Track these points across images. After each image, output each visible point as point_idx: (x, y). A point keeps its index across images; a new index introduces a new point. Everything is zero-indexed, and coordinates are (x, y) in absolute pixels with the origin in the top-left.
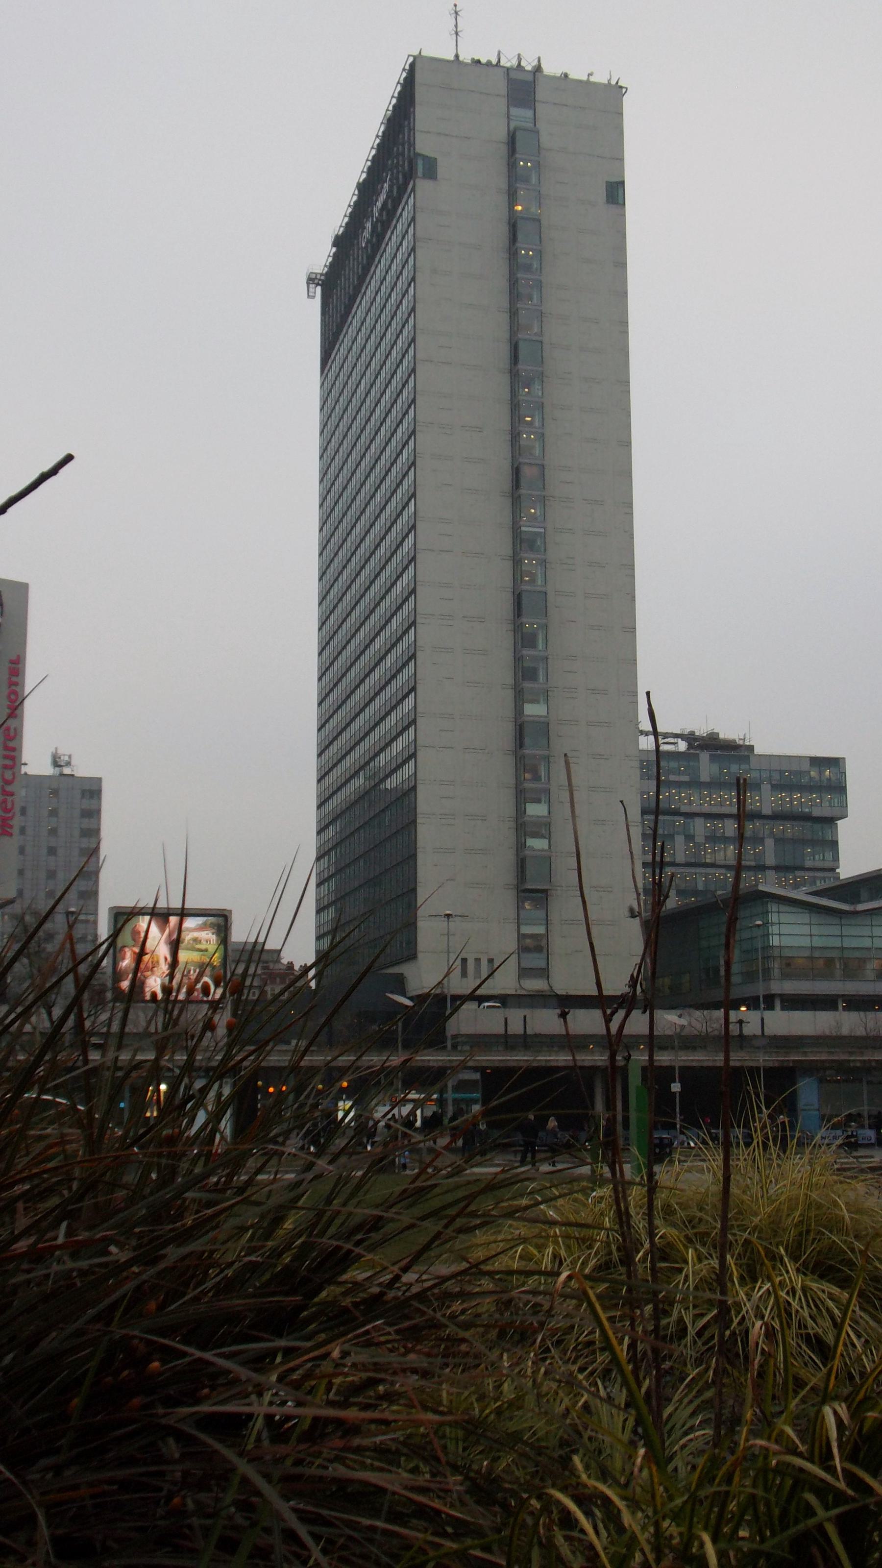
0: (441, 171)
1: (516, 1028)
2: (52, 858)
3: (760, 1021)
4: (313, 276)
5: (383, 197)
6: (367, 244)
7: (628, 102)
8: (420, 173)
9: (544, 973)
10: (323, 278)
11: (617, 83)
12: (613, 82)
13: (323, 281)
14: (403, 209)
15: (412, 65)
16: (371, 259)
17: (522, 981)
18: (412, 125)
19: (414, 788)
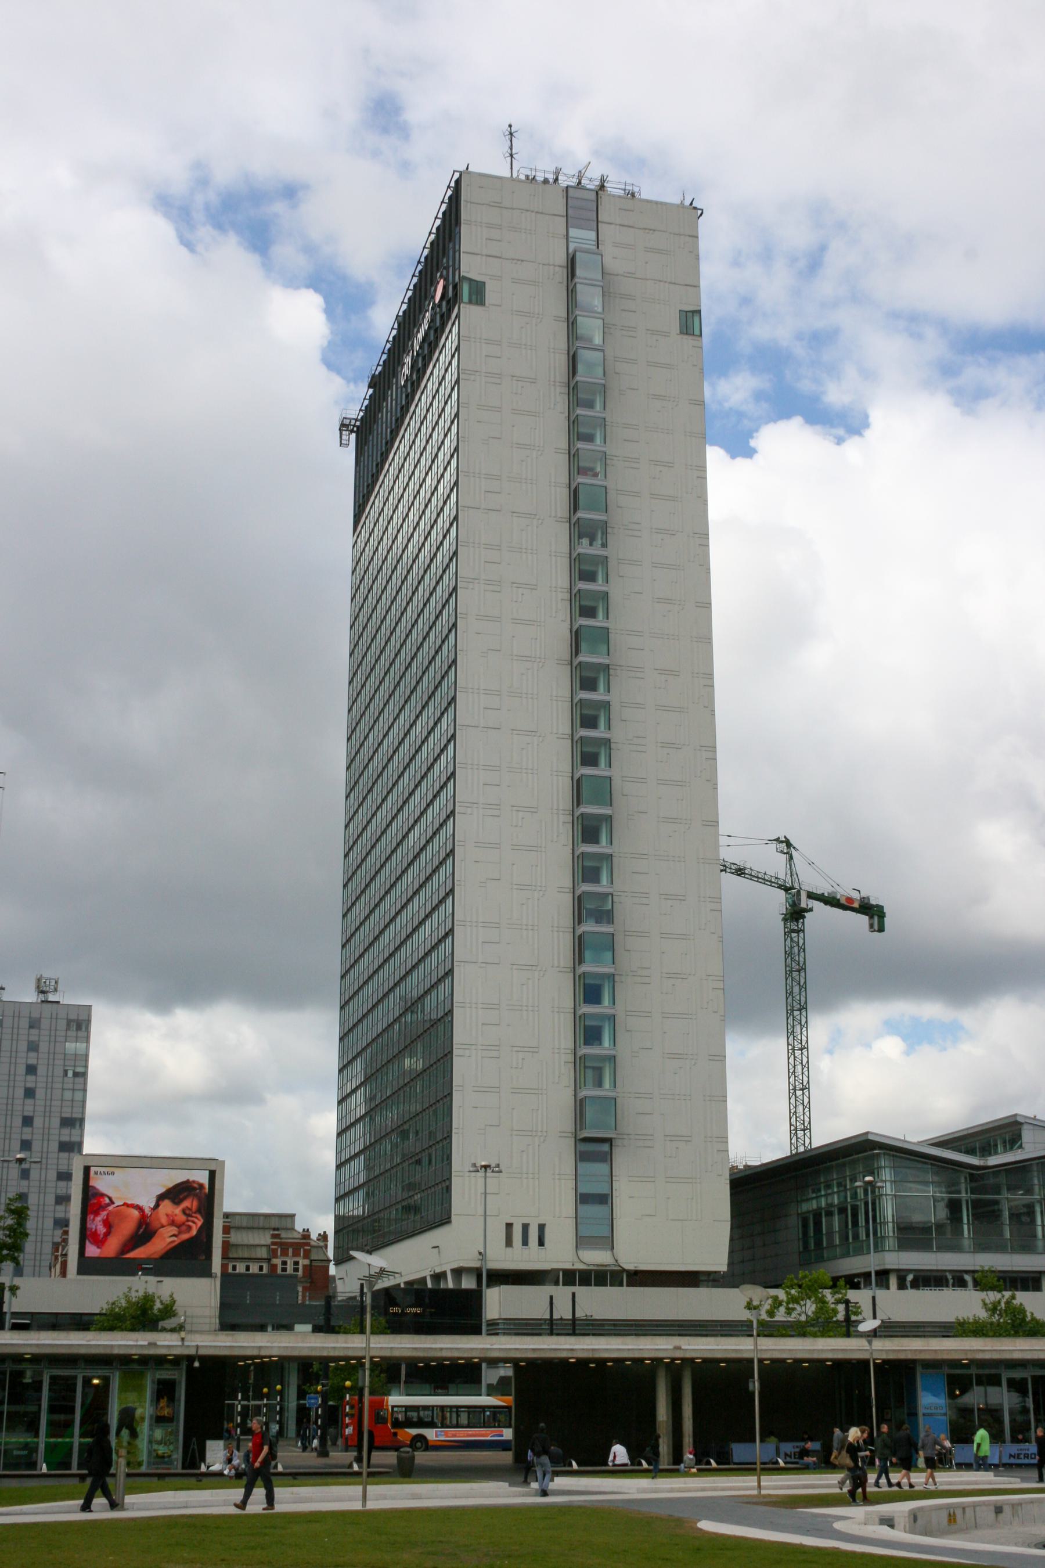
0: (490, 297)
1: (562, 1311)
2: (29, 1101)
3: (549, 1300)
4: (347, 422)
5: (425, 326)
6: (406, 381)
7: (704, 225)
8: (466, 298)
9: (608, 1242)
10: (358, 424)
11: (691, 204)
12: (687, 203)
13: (358, 427)
14: (447, 338)
15: (458, 182)
16: (410, 398)
17: (580, 1252)
18: (457, 247)
19: (451, 1012)
